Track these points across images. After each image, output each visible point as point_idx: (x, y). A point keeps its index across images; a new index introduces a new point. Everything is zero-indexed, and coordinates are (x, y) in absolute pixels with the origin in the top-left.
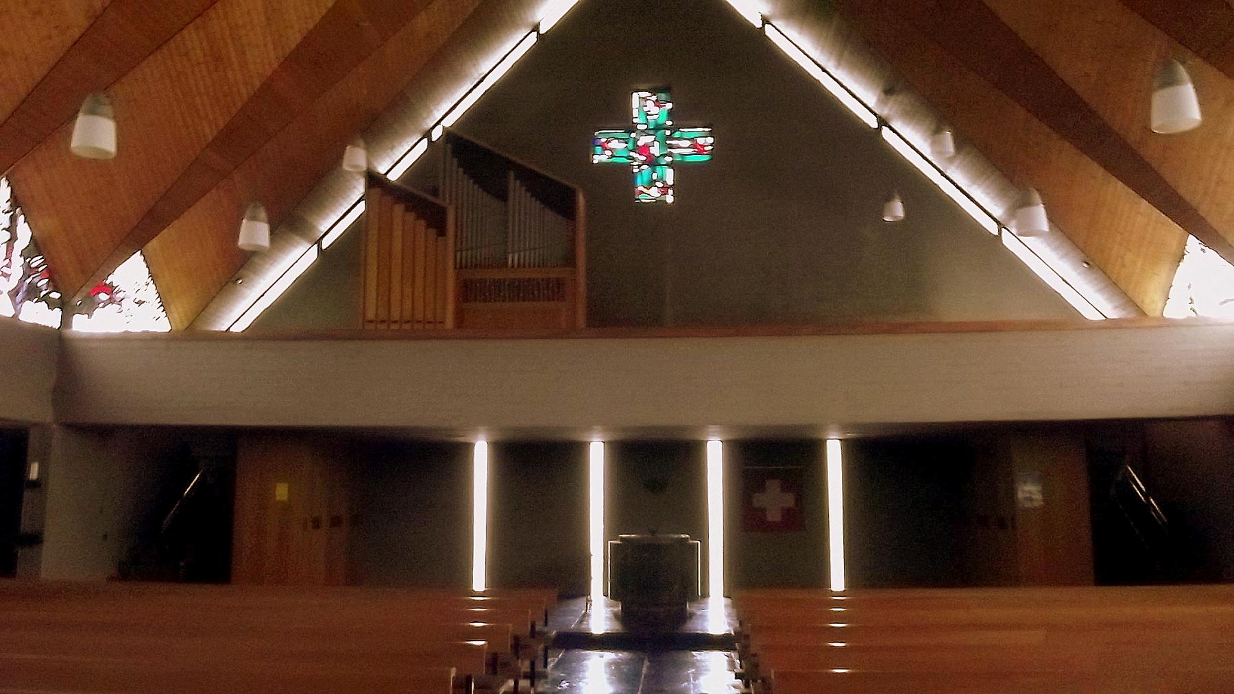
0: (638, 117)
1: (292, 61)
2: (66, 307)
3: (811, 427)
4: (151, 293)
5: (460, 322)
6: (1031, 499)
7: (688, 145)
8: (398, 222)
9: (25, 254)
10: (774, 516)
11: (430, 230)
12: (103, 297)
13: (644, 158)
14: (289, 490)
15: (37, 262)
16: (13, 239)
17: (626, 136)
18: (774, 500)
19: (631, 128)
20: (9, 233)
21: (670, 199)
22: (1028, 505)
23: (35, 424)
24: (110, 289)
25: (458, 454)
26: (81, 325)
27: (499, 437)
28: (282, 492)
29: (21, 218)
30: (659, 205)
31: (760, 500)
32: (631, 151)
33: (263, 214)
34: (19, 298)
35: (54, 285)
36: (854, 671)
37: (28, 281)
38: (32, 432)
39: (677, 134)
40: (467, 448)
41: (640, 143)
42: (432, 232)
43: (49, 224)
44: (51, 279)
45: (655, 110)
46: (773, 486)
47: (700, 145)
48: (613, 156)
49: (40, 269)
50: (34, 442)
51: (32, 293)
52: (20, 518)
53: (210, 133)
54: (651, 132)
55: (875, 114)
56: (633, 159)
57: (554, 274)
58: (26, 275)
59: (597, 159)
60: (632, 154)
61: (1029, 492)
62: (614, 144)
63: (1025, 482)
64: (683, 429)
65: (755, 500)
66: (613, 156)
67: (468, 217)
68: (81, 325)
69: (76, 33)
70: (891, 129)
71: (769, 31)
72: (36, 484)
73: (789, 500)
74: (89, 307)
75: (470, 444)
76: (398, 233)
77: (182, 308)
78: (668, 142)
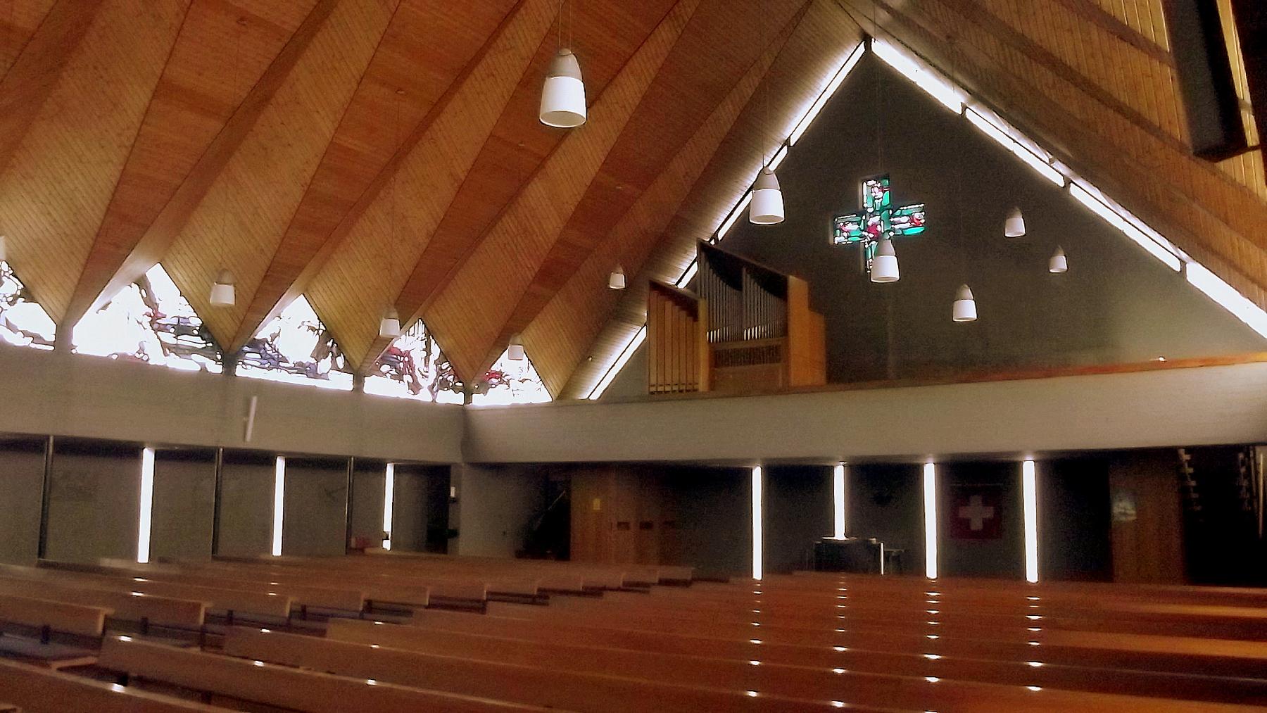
0: (868, 204)
3: (917, 456)
4: (532, 373)
5: (713, 384)
6: (1125, 514)
7: (906, 221)
10: (977, 525)
11: (688, 318)
15: (445, 366)
16: (429, 354)
17: (859, 218)
18: (977, 514)
19: (863, 212)
20: (425, 352)
22: (1123, 519)
23: (453, 464)
24: (499, 375)
25: (748, 474)
26: (479, 401)
28: (597, 504)
29: (433, 341)
31: (965, 513)
32: (862, 231)
33: (395, 315)
34: (435, 389)
37: (441, 378)
39: (898, 212)
40: (831, 470)
41: (870, 224)
42: (690, 318)
43: (449, 342)
44: (456, 375)
45: (880, 194)
46: (976, 501)
47: (917, 219)
48: (848, 237)
49: (448, 369)
50: (453, 471)
51: (444, 385)
53: (530, 275)
55: (1062, 175)
56: (865, 237)
58: (439, 375)
59: (837, 240)
60: (864, 233)
61: (1123, 508)
62: (850, 227)
63: (1121, 500)
66: (848, 237)
70: (1074, 183)
71: (969, 115)
72: (455, 500)
73: (989, 513)
74: (484, 387)
77: (556, 382)
78: (892, 220)
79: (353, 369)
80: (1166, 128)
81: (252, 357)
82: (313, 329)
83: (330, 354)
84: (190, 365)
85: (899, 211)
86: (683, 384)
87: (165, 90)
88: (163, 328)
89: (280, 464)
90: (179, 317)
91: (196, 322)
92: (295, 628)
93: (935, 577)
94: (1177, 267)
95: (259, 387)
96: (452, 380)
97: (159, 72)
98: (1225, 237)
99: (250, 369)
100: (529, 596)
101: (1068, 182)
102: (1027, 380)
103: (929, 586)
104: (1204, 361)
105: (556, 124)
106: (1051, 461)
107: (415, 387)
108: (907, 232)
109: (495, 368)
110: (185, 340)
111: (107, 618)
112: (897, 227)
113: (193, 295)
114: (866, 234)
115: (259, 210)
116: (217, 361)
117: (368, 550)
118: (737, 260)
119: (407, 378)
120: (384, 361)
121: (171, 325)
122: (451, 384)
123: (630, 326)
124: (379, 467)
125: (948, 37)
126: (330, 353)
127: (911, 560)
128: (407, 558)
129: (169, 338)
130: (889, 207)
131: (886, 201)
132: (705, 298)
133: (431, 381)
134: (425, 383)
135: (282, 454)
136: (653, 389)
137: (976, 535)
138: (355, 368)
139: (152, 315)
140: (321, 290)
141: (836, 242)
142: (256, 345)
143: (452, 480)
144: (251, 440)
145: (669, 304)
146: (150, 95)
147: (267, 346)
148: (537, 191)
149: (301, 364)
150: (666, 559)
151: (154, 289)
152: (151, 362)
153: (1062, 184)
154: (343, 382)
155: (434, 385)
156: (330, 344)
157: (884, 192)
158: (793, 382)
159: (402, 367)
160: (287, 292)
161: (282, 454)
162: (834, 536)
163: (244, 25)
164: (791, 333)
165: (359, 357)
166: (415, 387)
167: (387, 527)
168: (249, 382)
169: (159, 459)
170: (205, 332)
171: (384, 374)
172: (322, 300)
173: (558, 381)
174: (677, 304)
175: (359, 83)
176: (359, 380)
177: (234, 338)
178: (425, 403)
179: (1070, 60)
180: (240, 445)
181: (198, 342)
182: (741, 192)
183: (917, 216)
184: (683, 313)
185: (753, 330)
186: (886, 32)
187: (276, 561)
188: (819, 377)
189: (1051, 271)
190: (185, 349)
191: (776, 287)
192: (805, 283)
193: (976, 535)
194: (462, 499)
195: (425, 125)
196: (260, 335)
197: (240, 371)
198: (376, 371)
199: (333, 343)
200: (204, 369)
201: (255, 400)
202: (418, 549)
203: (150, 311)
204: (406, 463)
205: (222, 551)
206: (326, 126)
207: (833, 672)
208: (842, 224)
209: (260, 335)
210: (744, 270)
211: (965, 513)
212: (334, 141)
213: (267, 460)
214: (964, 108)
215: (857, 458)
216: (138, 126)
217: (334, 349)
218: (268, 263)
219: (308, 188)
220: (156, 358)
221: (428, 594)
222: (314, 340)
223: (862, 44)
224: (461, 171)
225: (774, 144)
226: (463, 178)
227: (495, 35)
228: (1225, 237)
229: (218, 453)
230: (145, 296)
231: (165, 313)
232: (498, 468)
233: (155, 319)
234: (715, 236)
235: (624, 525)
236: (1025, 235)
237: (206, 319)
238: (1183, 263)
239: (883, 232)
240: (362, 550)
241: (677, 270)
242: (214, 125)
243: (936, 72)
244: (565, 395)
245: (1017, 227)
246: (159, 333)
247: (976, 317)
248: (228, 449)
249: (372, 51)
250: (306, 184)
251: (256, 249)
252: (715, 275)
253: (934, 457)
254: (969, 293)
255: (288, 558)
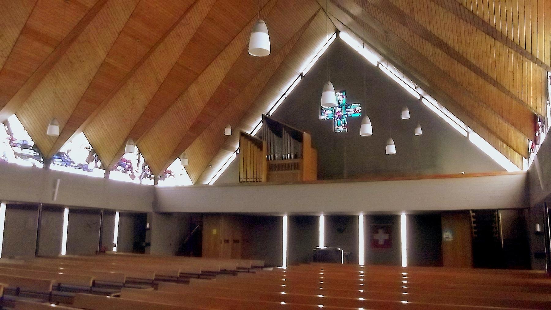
1: (209, 104)
2: (156, 180)
5: (268, 179)
8: (249, 147)
9: (144, 166)
10: (381, 242)
12: (168, 175)
13: (337, 116)
14: (217, 231)
15: (147, 167)
17: (332, 109)
18: (382, 237)
21: (346, 130)
22: (447, 240)
23: (148, 212)
24: (170, 172)
26: (161, 184)
27: (366, 214)
28: (215, 232)
29: (141, 156)
30: (342, 133)
31: (377, 237)
35: (152, 173)
36: (412, 303)
37: (144, 173)
38: (148, 214)
39: (349, 107)
40: (318, 217)
41: (337, 111)
42: (259, 150)
43: (149, 157)
44: (151, 171)
46: (381, 231)
49: (148, 169)
51: (145, 176)
52: (505, 269)
54: (340, 107)
57: (296, 161)
58: (143, 171)
59: (323, 117)
61: (447, 235)
63: (446, 232)
64: (277, 213)
65: (374, 236)
67: (286, 138)
68: (161, 184)
69: (142, 112)
71: (380, 66)
72: (149, 229)
73: (386, 237)
74: (163, 177)
75: (280, 217)
76: (249, 150)
77: (195, 176)
79: (105, 168)
80: (490, 74)
81: (58, 161)
82: (87, 148)
83: (94, 160)
84: (28, 163)
85: (350, 106)
86: (259, 179)
87: (26, 31)
88: (15, 145)
89: (66, 211)
90: (23, 141)
91: (31, 143)
92: (94, 291)
93: (363, 265)
94: (465, 135)
95: (61, 175)
96: (149, 174)
97: (24, 22)
98: (495, 121)
99: (56, 166)
100: (197, 275)
101: (422, 97)
102: (474, 178)
103: (404, 270)
104: (484, 174)
105: (255, 54)
106: (372, 215)
107: (132, 177)
108: (353, 116)
109: (168, 169)
110: (26, 152)
111: (4, 289)
112: (349, 113)
113: (30, 130)
114: (335, 115)
115: (67, 91)
116: (40, 161)
117: (107, 252)
118: (281, 125)
119: (129, 172)
120: (119, 164)
121: (19, 144)
122: (149, 176)
123: (228, 151)
124: (113, 213)
125: (385, 32)
126: (94, 160)
127: (352, 257)
128: (129, 256)
129: (18, 150)
130: (345, 104)
131: (344, 102)
132: (266, 141)
133: (140, 174)
134: (137, 175)
135: (68, 206)
136: (241, 180)
137: (382, 246)
138: (106, 167)
139: (10, 139)
140: (91, 130)
141: (322, 119)
142: (60, 155)
143: (148, 219)
144: (56, 200)
145: (249, 143)
146: (19, 33)
147: (65, 155)
148: (193, 90)
149: (80, 165)
150: (244, 257)
151: (11, 126)
152: (8, 162)
153: (419, 98)
154: (99, 174)
155: (141, 176)
156: (94, 155)
157: (343, 97)
158: (304, 180)
159: (127, 168)
160: (77, 131)
161: (68, 206)
162: (319, 247)
163: (68, 3)
164: (304, 157)
165: (108, 162)
166: (132, 177)
167: (115, 241)
168: (55, 172)
169: (9, 208)
170: (36, 148)
171: (118, 170)
172: (91, 135)
173: (195, 175)
174: (253, 143)
175: (119, 35)
176: (107, 171)
177: (50, 151)
178: (136, 184)
179: (451, 43)
180: (51, 202)
181: (32, 153)
182: (281, 94)
183: (357, 109)
184: (256, 147)
185: (271, 155)
186: (347, 28)
187: (64, 258)
188: (314, 177)
189: (415, 134)
190: (25, 156)
191: (298, 137)
192: (310, 135)
193: (382, 246)
194: (153, 229)
195: (146, 57)
196: (62, 150)
197: (52, 167)
198: (115, 168)
199: (96, 155)
200: (34, 166)
201: (59, 181)
202: (130, 252)
203: (9, 137)
204: (126, 212)
205: (41, 252)
206: (102, 54)
207: (318, 307)
208: (325, 111)
209: (62, 150)
210: (284, 129)
211: (377, 237)
212: (106, 61)
213: (59, 209)
214: (379, 64)
215: (417, 211)
216: (12, 47)
217: (96, 158)
218: (69, 116)
219: (91, 82)
220: (11, 159)
221: (154, 274)
222: (87, 153)
223: (336, 33)
224: (161, 78)
225: (296, 75)
226: (162, 81)
227: (182, 17)
228: (495, 121)
229: (40, 206)
230: (7, 129)
231: (16, 138)
232: (168, 215)
233: (11, 140)
234: (268, 113)
235: (227, 241)
236: (410, 118)
237: (36, 140)
238: (468, 133)
239: (342, 115)
240: (104, 252)
241: (251, 127)
242: (49, 50)
243: (369, 47)
244: (198, 183)
245: (406, 115)
246: (13, 147)
247: (395, 152)
248: (44, 204)
249: (126, 20)
250: (90, 80)
251: (64, 109)
252: (270, 131)
253: (324, 213)
254: (393, 142)
255: (68, 256)
